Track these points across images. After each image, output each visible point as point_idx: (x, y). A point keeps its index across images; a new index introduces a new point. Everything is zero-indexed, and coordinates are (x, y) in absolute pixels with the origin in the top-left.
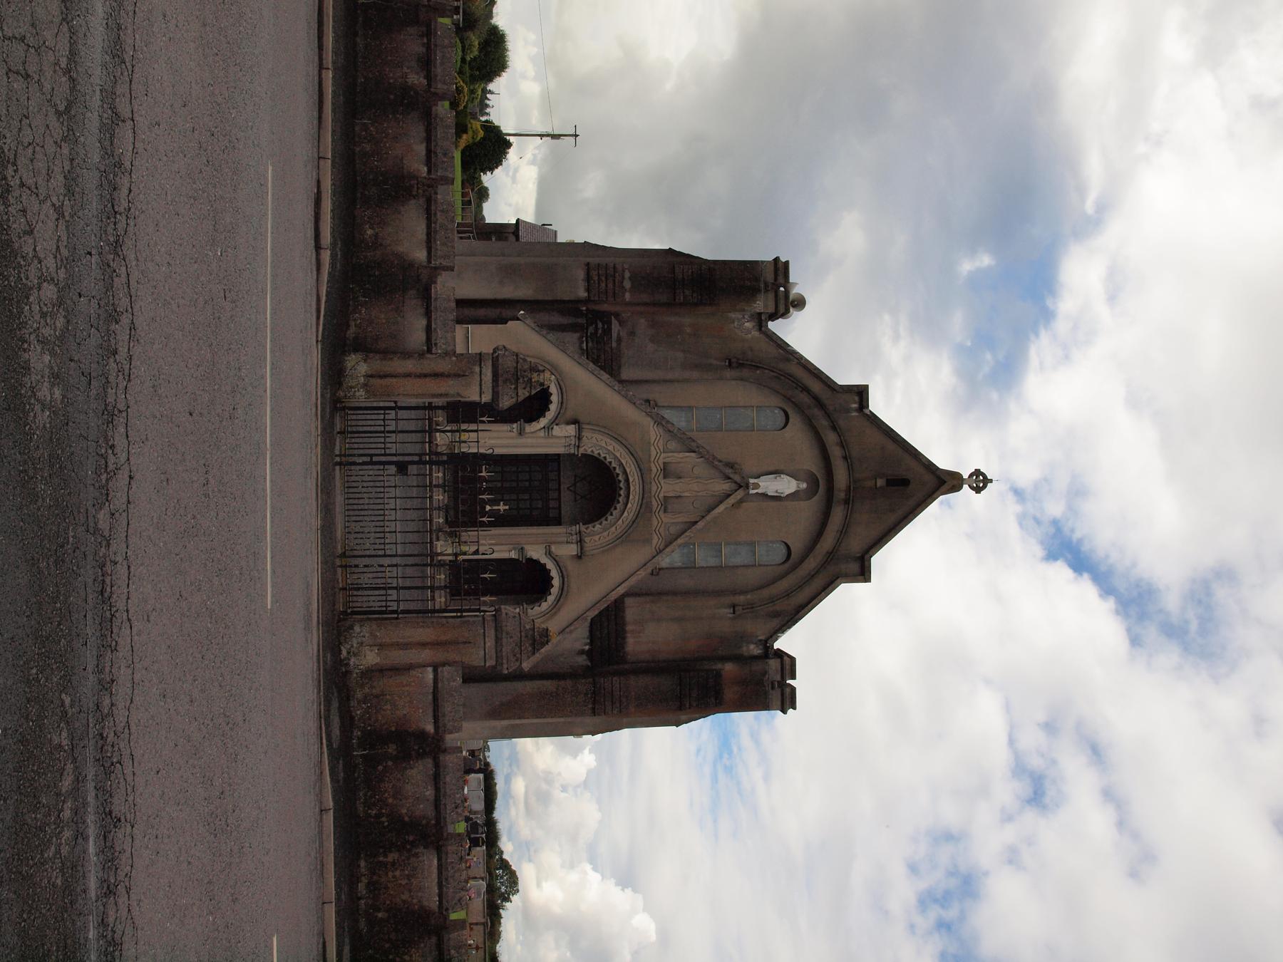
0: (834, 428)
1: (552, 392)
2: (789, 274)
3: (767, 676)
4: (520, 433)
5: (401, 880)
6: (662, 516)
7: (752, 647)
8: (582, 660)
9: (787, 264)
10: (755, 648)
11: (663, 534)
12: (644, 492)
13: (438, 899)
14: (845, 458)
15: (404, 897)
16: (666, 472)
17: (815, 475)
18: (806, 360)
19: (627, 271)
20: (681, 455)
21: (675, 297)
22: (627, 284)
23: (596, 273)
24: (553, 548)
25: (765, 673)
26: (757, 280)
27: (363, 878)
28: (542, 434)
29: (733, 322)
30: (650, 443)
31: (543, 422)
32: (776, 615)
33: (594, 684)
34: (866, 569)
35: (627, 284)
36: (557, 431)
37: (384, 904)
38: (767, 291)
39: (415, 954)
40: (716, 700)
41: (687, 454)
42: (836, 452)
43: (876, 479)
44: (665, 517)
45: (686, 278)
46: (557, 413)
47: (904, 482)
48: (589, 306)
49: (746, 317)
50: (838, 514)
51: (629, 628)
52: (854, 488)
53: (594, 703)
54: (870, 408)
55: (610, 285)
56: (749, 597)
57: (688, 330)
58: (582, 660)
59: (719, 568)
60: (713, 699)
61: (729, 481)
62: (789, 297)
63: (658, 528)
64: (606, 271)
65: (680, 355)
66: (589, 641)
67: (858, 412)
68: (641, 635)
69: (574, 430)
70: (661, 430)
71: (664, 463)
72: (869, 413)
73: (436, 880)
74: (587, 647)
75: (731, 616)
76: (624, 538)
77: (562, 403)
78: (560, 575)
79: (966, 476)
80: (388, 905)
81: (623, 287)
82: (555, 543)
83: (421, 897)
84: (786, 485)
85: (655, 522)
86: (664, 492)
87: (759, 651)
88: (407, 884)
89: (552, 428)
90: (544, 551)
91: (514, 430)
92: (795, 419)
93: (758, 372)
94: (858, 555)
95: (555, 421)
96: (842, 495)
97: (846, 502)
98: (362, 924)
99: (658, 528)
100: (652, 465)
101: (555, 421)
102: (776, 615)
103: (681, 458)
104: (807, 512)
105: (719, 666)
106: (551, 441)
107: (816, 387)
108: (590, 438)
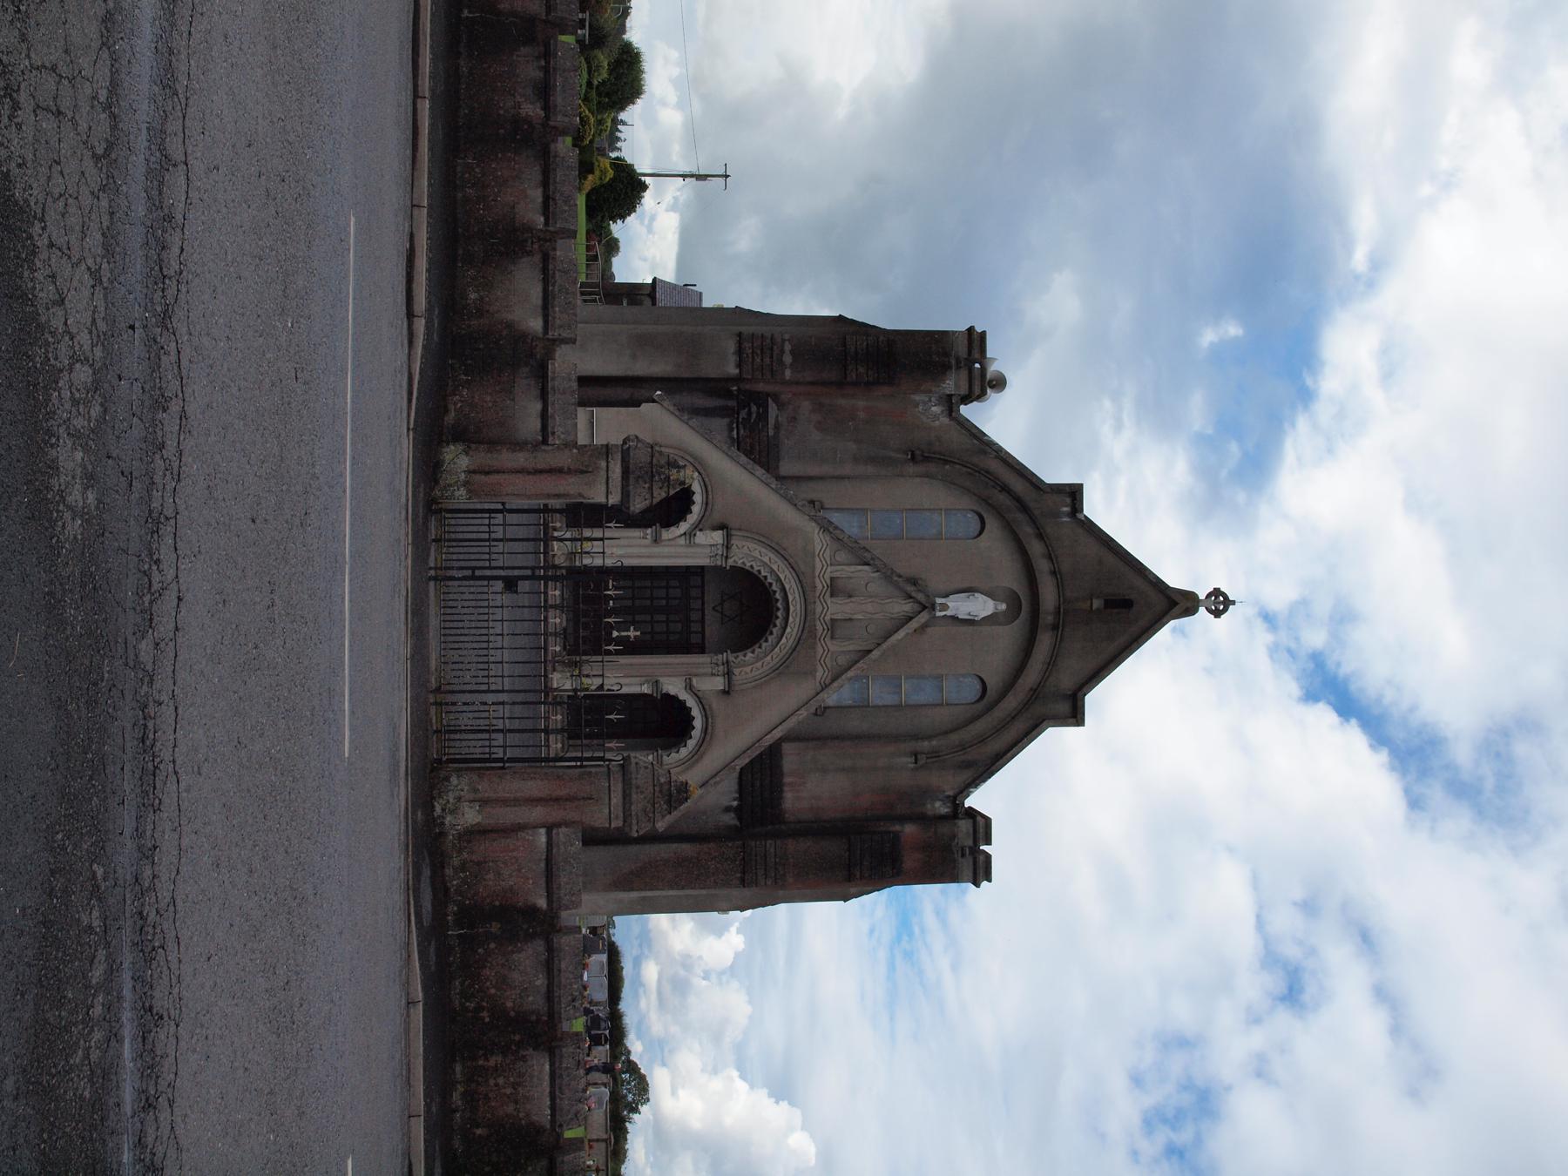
0: (1041, 536)
7: (938, 804)
8: (730, 819)
9: (983, 335)
10: (941, 806)
12: (807, 613)
13: (549, 1112)
14: (1054, 573)
18: (1007, 453)
19: (787, 343)
20: (853, 568)
22: (788, 359)
24: (694, 681)
25: (954, 837)
28: (682, 541)
29: (917, 405)
31: (684, 527)
35: (788, 359)
36: (701, 538)
38: (958, 368)
40: (893, 868)
41: (860, 567)
42: (1042, 566)
43: (1092, 600)
49: (933, 399)
50: (1045, 642)
51: (787, 780)
52: (1064, 610)
53: (744, 873)
56: (934, 743)
57: (862, 415)
58: (730, 819)
59: (898, 707)
61: (911, 600)
70: (828, 538)
74: (735, 803)
75: (912, 766)
76: (781, 670)
79: (1202, 596)
82: (696, 675)
84: (980, 606)
89: (695, 535)
90: (684, 685)
92: (992, 524)
93: (947, 467)
95: (698, 526)
96: (1050, 619)
97: (1055, 627)
100: (817, 581)
102: (967, 765)
103: (853, 572)
104: (1007, 639)
105: (897, 828)
107: (1018, 486)
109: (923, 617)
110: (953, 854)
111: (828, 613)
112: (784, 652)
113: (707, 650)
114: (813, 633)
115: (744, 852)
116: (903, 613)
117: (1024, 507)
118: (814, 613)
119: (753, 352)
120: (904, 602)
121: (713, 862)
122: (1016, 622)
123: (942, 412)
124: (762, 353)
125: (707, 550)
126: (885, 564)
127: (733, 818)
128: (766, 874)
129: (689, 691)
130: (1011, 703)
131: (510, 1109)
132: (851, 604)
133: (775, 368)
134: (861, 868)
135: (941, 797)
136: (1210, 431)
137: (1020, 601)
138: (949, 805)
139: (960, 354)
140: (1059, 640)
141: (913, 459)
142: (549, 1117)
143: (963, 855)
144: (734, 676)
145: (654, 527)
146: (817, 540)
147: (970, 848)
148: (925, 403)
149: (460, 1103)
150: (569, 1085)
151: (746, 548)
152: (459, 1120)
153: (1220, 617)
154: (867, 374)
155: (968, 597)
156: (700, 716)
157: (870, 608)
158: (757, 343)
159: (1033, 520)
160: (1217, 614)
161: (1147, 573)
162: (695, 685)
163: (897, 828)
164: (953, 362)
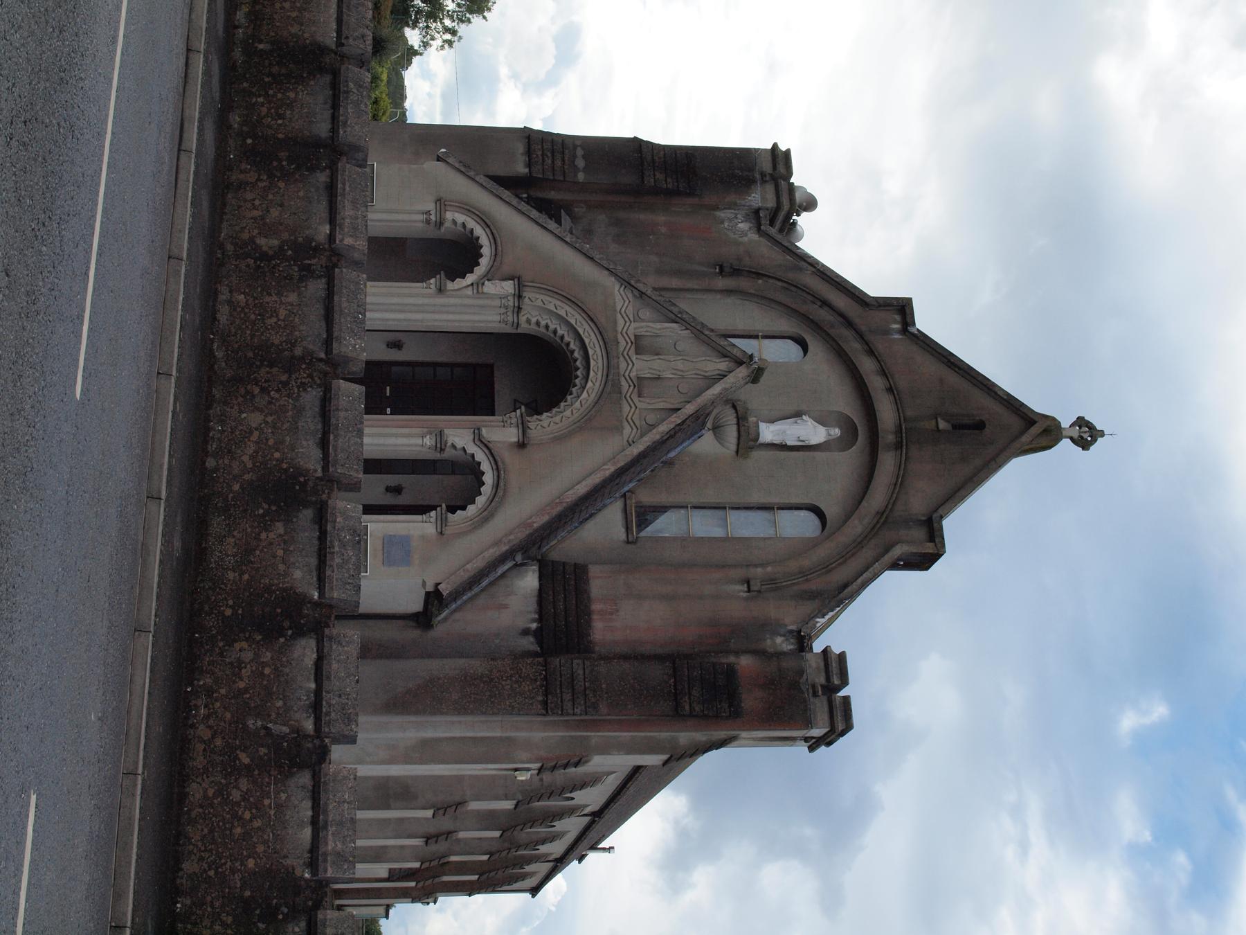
0: (871, 352)
1: (478, 235)
2: (791, 163)
3: (805, 677)
4: (441, 533)
5: (291, 11)
6: (636, 399)
7: (779, 640)
8: (529, 643)
9: (842, 657)
10: (783, 642)
11: (637, 422)
12: (609, 367)
13: (335, 35)
14: (890, 390)
15: (293, 31)
16: (639, 345)
17: (852, 420)
18: (823, 266)
19: (579, 148)
20: (658, 325)
21: (643, 178)
22: (580, 163)
23: (540, 147)
24: (484, 431)
25: (801, 672)
26: (751, 170)
27: (243, 6)
28: (469, 292)
29: (722, 222)
30: (615, 310)
31: (470, 278)
32: (812, 596)
33: (546, 664)
34: (937, 533)
35: (580, 163)
36: (489, 287)
37: (268, 35)
38: (764, 182)
39: (303, 91)
40: (730, 707)
41: (667, 325)
42: (876, 384)
43: (936, 419)
44: (640, 401)
45: (656, 158)
46: (489, 266)
47: (980, 426)
48: (532, 193)
49: (739, 216)
50: (888, 462)
51: (596, 607)
52: (906, 429)
53: (546, 694)
54: (917, 327)
55: (558, 163)
56: (769, 569)
57: (663, 230)
58: (529, 643)
59: (726, 539)
60: (726, 705)
61: (727, 359)
62: (795, 200)
63: (631, 415)
64: (553, 147)
65: (654, 258)
66: (537, 616)
67: (901, 334)
68: (614, 617)
69: (512, 286)
70: (630, 295)
71: (635, 336)
72: (916, 333)
73: (335, 16)
74: (534, 626)
75: (745, 595)
76: (585, 424)
77: (496, 255)
78: (494, 467)
79: (1065, 424)
80: (272, 37)
81: (576, 166)
82: (486, 426)
83: (314, 32)
84: (812, 432)
85: (626, 408)
86: (637, 371)
87: (791, 647)
88: (297, 17)
89: (483, 284)
90: (472, 437)
91: (431, 286)
92: (814, 345)
93: (760, 281)
94: (923, 518)
95: (489, 276)
96: (891, 438)
97: (898, 446)
98: (238, 55)
99: (631, 415)
100: (620, 336)
101: (489, 276)
102: (812, 596)
103: (660, 329)
104: (846, 464)
105: (732, 659)
106: (481, 302)
107: (840, 301)
108: (533, 299)
109: (740, 372)
110: (803, 693)
111: (634, 369)
112: (585, 406)
113: (496, 413)
114: (617, 388)
115: (546, 671)
116: (717, 372)
117: (849, 323)
118: (618, 368)
119: (543, 155)
120: (717, 361)
121: (509, 682)
122: (854, 447)
123: (750, 228)
124: (553, 155)
125: (497, 302)
126: (693, 318)
127: (532, 643)
128: (573, 700)
129: (478, 443)
130: (856, 527)
131: (294, 29)
132: (659, 361)
133: (567, 171)
134: (690, 698)
135: (782, 631)
136: (1147, 836)
137: (856, 428)
138: (792, 640)
139: (764, 169)
140: (903, 459)
141: (722, 270)
142: (335, 39)
143: (815, 694)
144: (529, 431)
145: (438, 276)
146: (618, 297)
147: (822, 686)
148: (730, 220)
149: (243, 21)
150: (358, 8)
151: (539, 427)
152: (241, 35)
153: (1088, 449)
154: (666, 181)
155: (796, 422)
156: (491, 472)
157: (680, 365)
158: (547, 146)
159: (860, 336)
160: (1084, 444)
161: (996, 390)
162: (485, 436)
163: (732, 659)
164: (758, 176)
